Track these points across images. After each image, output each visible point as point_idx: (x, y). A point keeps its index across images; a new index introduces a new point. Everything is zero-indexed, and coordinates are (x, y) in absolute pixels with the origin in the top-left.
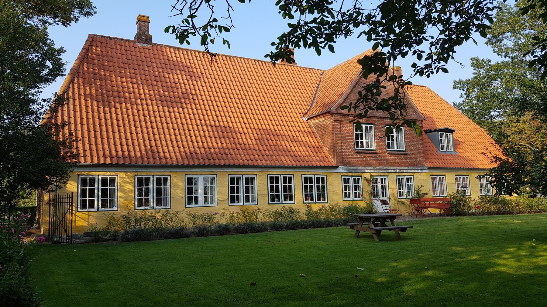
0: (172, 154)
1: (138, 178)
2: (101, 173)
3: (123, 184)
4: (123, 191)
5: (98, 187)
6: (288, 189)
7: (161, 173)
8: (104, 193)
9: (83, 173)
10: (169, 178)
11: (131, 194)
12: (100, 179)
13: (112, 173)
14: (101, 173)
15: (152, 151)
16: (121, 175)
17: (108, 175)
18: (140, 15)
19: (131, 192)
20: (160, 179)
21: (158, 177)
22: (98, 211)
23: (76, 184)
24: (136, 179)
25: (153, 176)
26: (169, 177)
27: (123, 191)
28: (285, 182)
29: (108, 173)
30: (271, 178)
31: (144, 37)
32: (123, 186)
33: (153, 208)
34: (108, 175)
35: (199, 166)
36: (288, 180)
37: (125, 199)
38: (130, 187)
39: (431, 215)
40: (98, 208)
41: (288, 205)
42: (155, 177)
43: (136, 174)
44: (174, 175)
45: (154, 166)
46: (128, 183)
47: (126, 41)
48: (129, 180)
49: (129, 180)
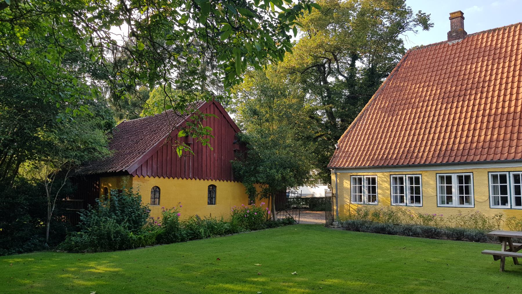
0: (426, 153)
1: (393, 177)
2: (365, 174)
3: (381, 183)
4: (382, 189)
5: (365, 184)
6: (465, 191)
7: (463, 170)
8: (504, 190)
9: (353, 174)
10: (420, 177)
11: (387, 192)
12: (365, 178)
13: (372, 174)
14: (365, 174)
15: (452, 150)
16: (379, 174)
17: (370, 174)
18: (451, 14)
19: (388, 190)
20: (462, 176)
21: (410, 176)
22: (511, 208)
23: (349, 183)
24: (392, 178)
25: (407, 174)
26: (471, 174)
27: (382, 189)
28: (461, 182)
29: (369, 174)
30: (396, 179)
31: (454, 34)
32: (381, 184)
33: (406, 205)
34: (370, 174)
35: (425, 165)
36: (465, 180)
37: (383, 195)
38: (387, 185)
39: (309, 226)
40: (511, 205)
41: (467, 210)
42: (511, 173)
43: (391, 173)
44: (424, 174)
45: (408, 166)
46: (386, 182)
47: (441, 43)
48: (385, 179)
49: (385, 179)
